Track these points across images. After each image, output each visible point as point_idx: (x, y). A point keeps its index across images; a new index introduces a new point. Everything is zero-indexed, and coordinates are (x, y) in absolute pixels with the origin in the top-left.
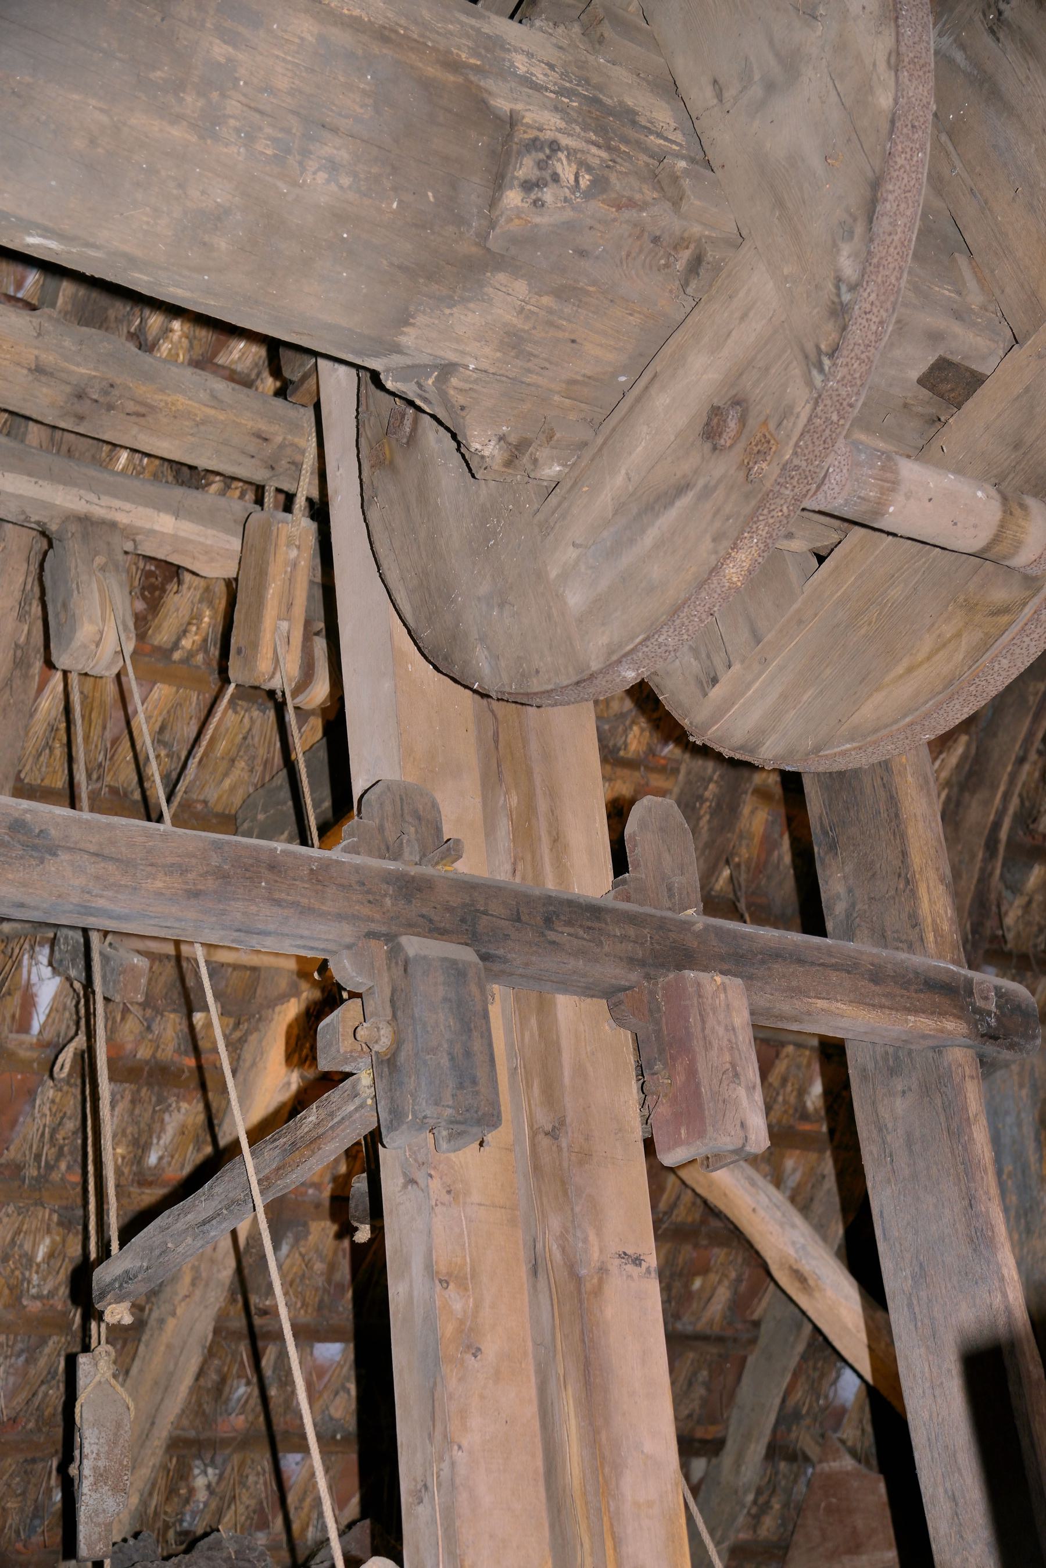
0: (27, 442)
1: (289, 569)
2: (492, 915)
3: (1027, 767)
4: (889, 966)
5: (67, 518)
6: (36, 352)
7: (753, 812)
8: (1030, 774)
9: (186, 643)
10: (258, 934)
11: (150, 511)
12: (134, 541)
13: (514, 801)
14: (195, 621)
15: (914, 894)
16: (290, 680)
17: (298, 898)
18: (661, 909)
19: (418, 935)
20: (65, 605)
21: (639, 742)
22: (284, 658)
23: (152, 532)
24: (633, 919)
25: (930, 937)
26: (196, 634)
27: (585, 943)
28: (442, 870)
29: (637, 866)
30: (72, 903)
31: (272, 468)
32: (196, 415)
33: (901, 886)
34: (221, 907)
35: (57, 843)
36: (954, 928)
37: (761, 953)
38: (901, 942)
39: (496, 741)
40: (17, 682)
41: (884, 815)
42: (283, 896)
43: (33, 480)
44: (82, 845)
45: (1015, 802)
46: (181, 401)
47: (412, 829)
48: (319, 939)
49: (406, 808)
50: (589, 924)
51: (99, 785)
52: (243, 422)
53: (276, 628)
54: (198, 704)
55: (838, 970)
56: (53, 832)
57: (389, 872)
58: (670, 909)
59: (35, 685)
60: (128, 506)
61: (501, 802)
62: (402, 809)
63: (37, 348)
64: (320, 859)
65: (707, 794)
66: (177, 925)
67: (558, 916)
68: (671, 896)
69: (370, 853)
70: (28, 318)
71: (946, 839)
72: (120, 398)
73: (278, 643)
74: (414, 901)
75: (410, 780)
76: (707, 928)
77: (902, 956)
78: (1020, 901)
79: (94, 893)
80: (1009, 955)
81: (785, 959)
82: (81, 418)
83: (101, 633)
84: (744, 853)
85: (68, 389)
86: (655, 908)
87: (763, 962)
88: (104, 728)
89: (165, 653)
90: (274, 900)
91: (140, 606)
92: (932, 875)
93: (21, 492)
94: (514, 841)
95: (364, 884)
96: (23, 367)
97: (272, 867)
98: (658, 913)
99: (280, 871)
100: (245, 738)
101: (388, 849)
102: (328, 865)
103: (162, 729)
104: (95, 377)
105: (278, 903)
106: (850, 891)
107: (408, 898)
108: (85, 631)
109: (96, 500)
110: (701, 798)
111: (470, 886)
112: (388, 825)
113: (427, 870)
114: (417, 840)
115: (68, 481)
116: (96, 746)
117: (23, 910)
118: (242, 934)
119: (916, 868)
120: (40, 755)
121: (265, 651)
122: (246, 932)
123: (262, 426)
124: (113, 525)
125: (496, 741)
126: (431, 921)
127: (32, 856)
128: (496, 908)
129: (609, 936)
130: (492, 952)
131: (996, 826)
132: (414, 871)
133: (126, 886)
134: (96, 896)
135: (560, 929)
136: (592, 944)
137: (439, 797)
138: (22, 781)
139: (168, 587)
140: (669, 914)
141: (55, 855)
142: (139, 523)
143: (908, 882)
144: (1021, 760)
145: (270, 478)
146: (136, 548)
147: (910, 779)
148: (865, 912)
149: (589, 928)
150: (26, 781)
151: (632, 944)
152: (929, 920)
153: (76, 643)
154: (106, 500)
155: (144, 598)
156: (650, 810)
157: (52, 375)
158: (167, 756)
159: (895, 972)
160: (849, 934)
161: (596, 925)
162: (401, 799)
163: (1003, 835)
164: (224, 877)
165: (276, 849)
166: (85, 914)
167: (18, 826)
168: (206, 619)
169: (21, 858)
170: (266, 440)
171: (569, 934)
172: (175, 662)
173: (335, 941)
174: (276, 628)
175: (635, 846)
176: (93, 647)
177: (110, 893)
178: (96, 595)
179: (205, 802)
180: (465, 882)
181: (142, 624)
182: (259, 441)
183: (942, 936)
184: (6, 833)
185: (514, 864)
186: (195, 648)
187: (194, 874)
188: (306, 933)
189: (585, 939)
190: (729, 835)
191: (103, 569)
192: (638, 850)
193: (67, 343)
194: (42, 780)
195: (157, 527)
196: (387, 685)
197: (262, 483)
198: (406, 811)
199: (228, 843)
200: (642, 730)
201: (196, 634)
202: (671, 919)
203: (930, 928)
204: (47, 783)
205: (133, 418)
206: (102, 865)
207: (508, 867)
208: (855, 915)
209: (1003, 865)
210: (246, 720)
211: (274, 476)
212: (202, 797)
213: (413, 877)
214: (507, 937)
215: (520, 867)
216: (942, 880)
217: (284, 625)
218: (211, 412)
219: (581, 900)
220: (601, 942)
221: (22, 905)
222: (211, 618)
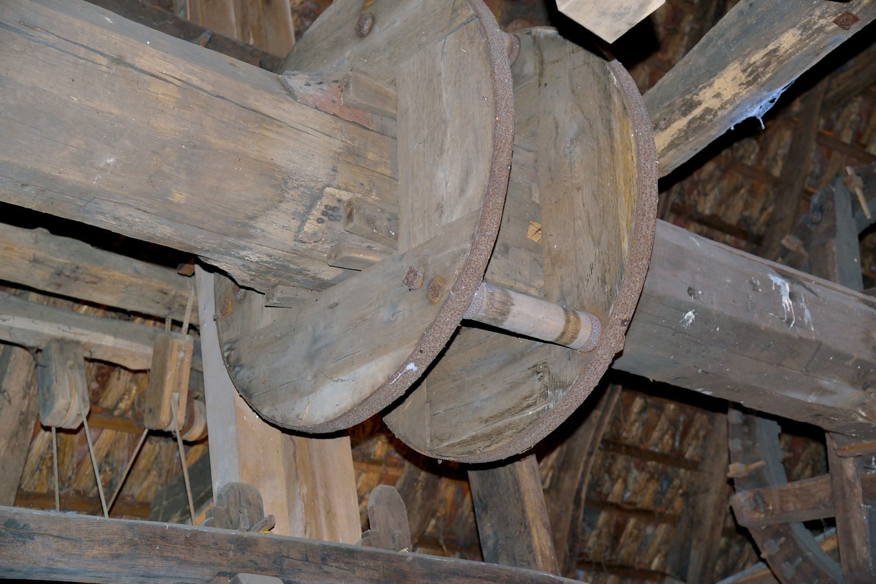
0: (30, 300)
1: (179, 364)
2: (292, 558)
3: (593, 458)
4: (517, 577)
5: (51, 340)
6: (34, 251)
7: (446, 487)
8: (595, 461)
9: (122, 406)
10: (154, 577)
11: (99, 334)
12: (90, 352)
13: (305, 490)
14: (127, 393)
15: (529, 534)
16: (179, 425)
17: (179, 555)
18: (389, 549)
19: (248, 572)
20: (48, 389)
21: (382, 450)
22: (176, 413)
23: (100, 346)
24: (373, 556)
25: (539, 558)
26: (128, 400)
27: (345, 571)
28: (264, 533)
29: (374, 525)
30: (42, 567)
31: (170, 309)
32: (126, 282)
33: (523, 530)
34: (132, 563)
35: (34, 531)
36: (552, 552)
37: (445, 572)
38: (524, 562)
39: (295, 457)
40: (21, 433)
41: (512, 490)
42: (169, 554)
43: (32, 320)
44: (50, 532)
45: (588, 477)
46: (117, 274)
47: (246, 510)
48: (191, 578)
49: (242, 498)
50: (348, 560)
51: (68, 490)
52: (153, 284)
53: (171, 397)
54: (129, 439)
55: (488, 580)
56: (32, 525)
57: (232, 536)
58: (393, 549)
59: (31, 434)
60: (86, 332)
61: (298, 491)
62: (240, 499)
63: (34, 249)
64: (191, 531)
65: (420, 478)
66: (105, 575)
67: (330, 556)
68: (394, 542)
69: (221, 526)
70: (30, 233)
71: (546, 502)
72: (82, 274)
73: (173, 405)
74: (246, 553)
75: (245, 482)
76: (414, 559)
77: (524, 570)
78: (594, 533)
79: (56, 559)
80: (589, 563)
81: (458, 575)
82: (59, 286)
83: (69, 404)
84: (442, 511)
85: (52, 270)
86: (386, 549)
87: (446, 577)
88: (72, 456)
89: (109, 412)
90: (164, 557)
91: (95, 385)
92: (539, 523)
93: (24, 327)
94: (305, 514)
95: (217, 544)
96: (26, 260)
97: (163, 538)
98: (387, 552)
99: (168, 540)
100: (156, 458)
101: (231, 522)
102: (196, 535)
103: (107, 455)
104: (68, 264)
105: (166, 558)
106: (495, 533)
107: (243, 551)
108: (60, 403)
109: (68, 329)
110: (417, 481)
111: (279, 542)
112: (231, 509)
113: (254, 534)
114: (248, 517)
115: (53, 320)
116: (68, 467)
117: (12, 573)
118: (145, 578)
119: (530, 519)
120: (34, 475)
121: (165, 410)
122: (147, 577)
123: (164, 286)
124: (78, 343)
125: (295, 457)
126: (256, 563)
127: (18, 541)
128: (294, 554)
129: (359, 566)
130: (292, 580)
131: (579, 491)
132: (246, 534)
133: (75, 554)
134: (57, 561)
135: (331, 564)
136: (349, 572)
137: (261, 491)
138: (22, 490)
139: (112, 374)
140: (393, 552)
141: (33, 539)
142: (93, 341)
143: (526, 527)
144: (590, 454)
145: (168, 314)
146: (91, 355)
147: (525, 469)
148: (504, 545)
149: (347, 563)
150: (25, 490)
151: (372, 571)
152: (538, 549)
153: (55, 411)
154: (74, 329)
155: (97, 381)
156: (381, 492)
157: (42, 263)
158: (110, 470)
159: (520, 580)
160: (495, 559)
161: (352, 560)
162: (240, 493)
163: (583, 495)
164: (134, 545)
165: (166, 526)
166: (50, 573)
167: (10, 523)
168: (134, 392)
169: (12, 542)
170: (166, 293)
171: (336, 567)
172: (115, 417)
173: (200, 579)
174: (171, 397)
175: (373, 513)
176: (64, 412)
177: (65, 559)
178: (67, 382)
179: (132, 496)
180: (276, 540)
181: (95, 399)
182: (161, 294)
183: (546, 558)
184: (2, 528)
185: (306, 527)
186: (127, 408)
187: (116, 544)
188: (183, 575)
189: (345, 569)
190: (433, 501)
191: (71, 368)
192: (375, 516)
193: (52, 246)
194: (35, 489)
195: (104, 343)
196: (232, 428)
197: (164, 317)
198: (242, 500)
199: (137, 525)
200: (383, 443)
201: (128, 400)
202: (394, 555)
203: (539, 553)
204: (38, 490)
205: (90, 285)
206: (61, 543)
207: (302, 529)
208: (498, 547)
209: (585, 512)
210: (157, 448)
211: (171, 313)
212: (130, 493)
213: (246, 538)
214: (300, 570)
215: (309, 528)
216: (544, 525)
217: (176, 395)
218: (134, 280)
219: (343, 547)
220: (354, 570)
221: (11, 570)
222: (137, 390)
